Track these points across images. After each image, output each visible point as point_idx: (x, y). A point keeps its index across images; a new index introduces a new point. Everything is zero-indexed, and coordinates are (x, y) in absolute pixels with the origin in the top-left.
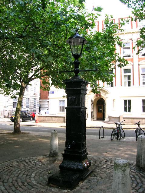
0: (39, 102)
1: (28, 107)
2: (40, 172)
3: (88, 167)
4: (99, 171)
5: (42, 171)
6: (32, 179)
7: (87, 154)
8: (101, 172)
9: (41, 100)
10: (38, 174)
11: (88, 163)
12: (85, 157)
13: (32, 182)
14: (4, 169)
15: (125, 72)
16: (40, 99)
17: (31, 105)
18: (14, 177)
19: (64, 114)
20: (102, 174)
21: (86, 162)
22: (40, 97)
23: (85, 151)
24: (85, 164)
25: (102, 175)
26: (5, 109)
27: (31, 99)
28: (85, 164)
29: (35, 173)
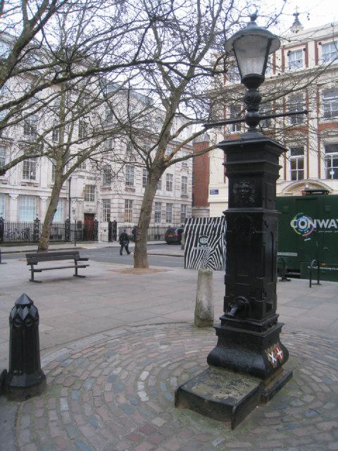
0: (190, 211)
1: (170, 221)
2: (164, 365)
3: (280, 364)
4: (308, 373)
5: (169, 363)
6: (141, 386)
7: (279, 330)
8: (313, 377)
9: (195, 208)
10: (157, 370)
11: (280, 353)
12: (274, 338)
13: (138, 393)
14: (85, 352)
15: (327, 151)
16: (193, 205)
17: (176, 217)
18: (100, 375)
19: (51, 190)
20: (318, 383)
21: (275, 352)
22: (193, 202)
23: (275, 322)
24: (272, 356)
25: (317, 389)
26: (127, 224)
27: (176, 206)
28: (272, 356)
29: (149, 368)
